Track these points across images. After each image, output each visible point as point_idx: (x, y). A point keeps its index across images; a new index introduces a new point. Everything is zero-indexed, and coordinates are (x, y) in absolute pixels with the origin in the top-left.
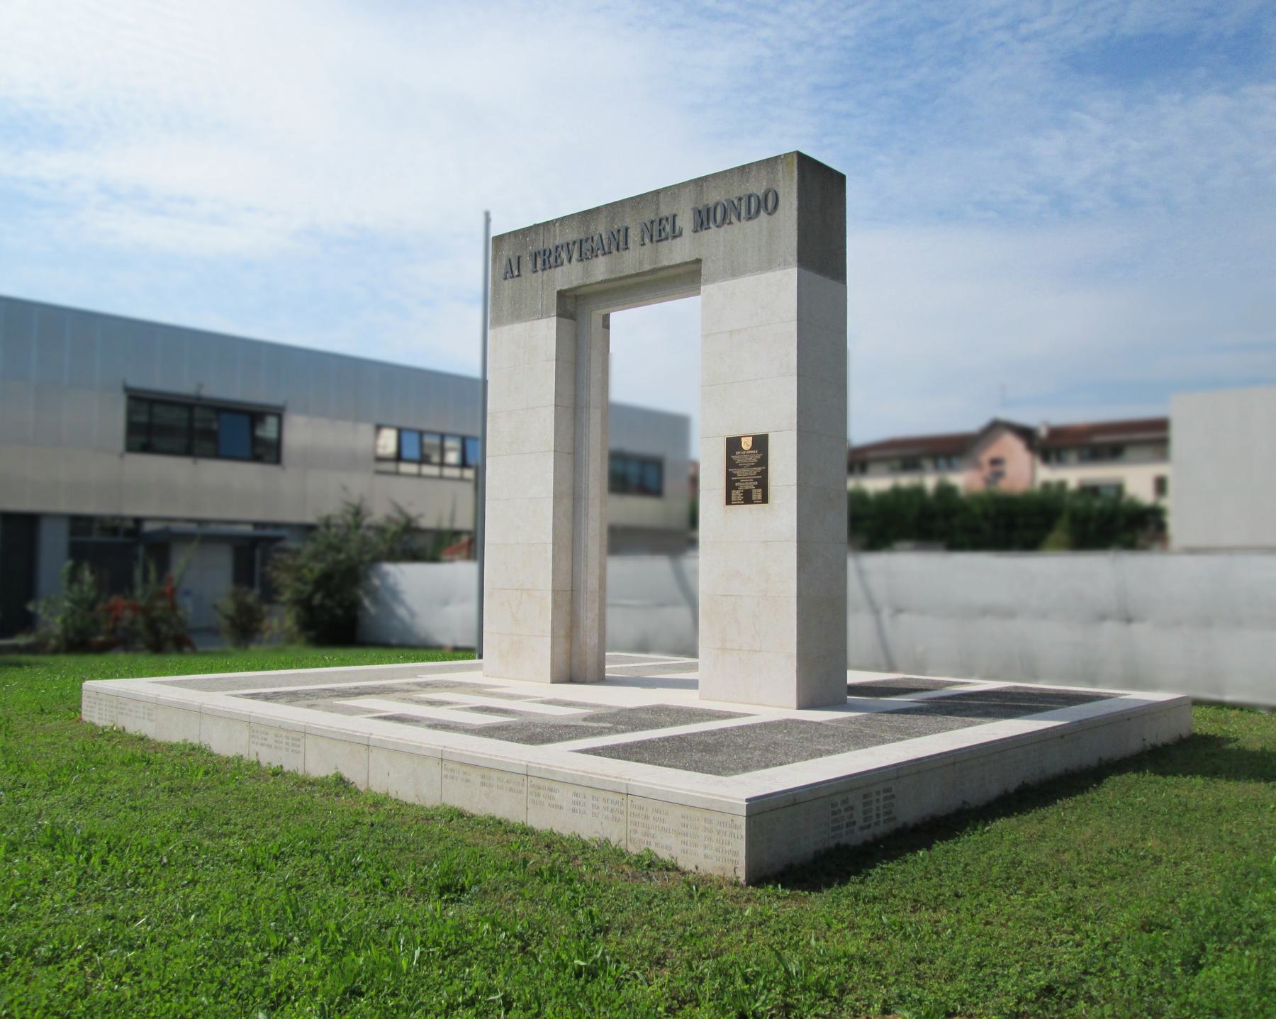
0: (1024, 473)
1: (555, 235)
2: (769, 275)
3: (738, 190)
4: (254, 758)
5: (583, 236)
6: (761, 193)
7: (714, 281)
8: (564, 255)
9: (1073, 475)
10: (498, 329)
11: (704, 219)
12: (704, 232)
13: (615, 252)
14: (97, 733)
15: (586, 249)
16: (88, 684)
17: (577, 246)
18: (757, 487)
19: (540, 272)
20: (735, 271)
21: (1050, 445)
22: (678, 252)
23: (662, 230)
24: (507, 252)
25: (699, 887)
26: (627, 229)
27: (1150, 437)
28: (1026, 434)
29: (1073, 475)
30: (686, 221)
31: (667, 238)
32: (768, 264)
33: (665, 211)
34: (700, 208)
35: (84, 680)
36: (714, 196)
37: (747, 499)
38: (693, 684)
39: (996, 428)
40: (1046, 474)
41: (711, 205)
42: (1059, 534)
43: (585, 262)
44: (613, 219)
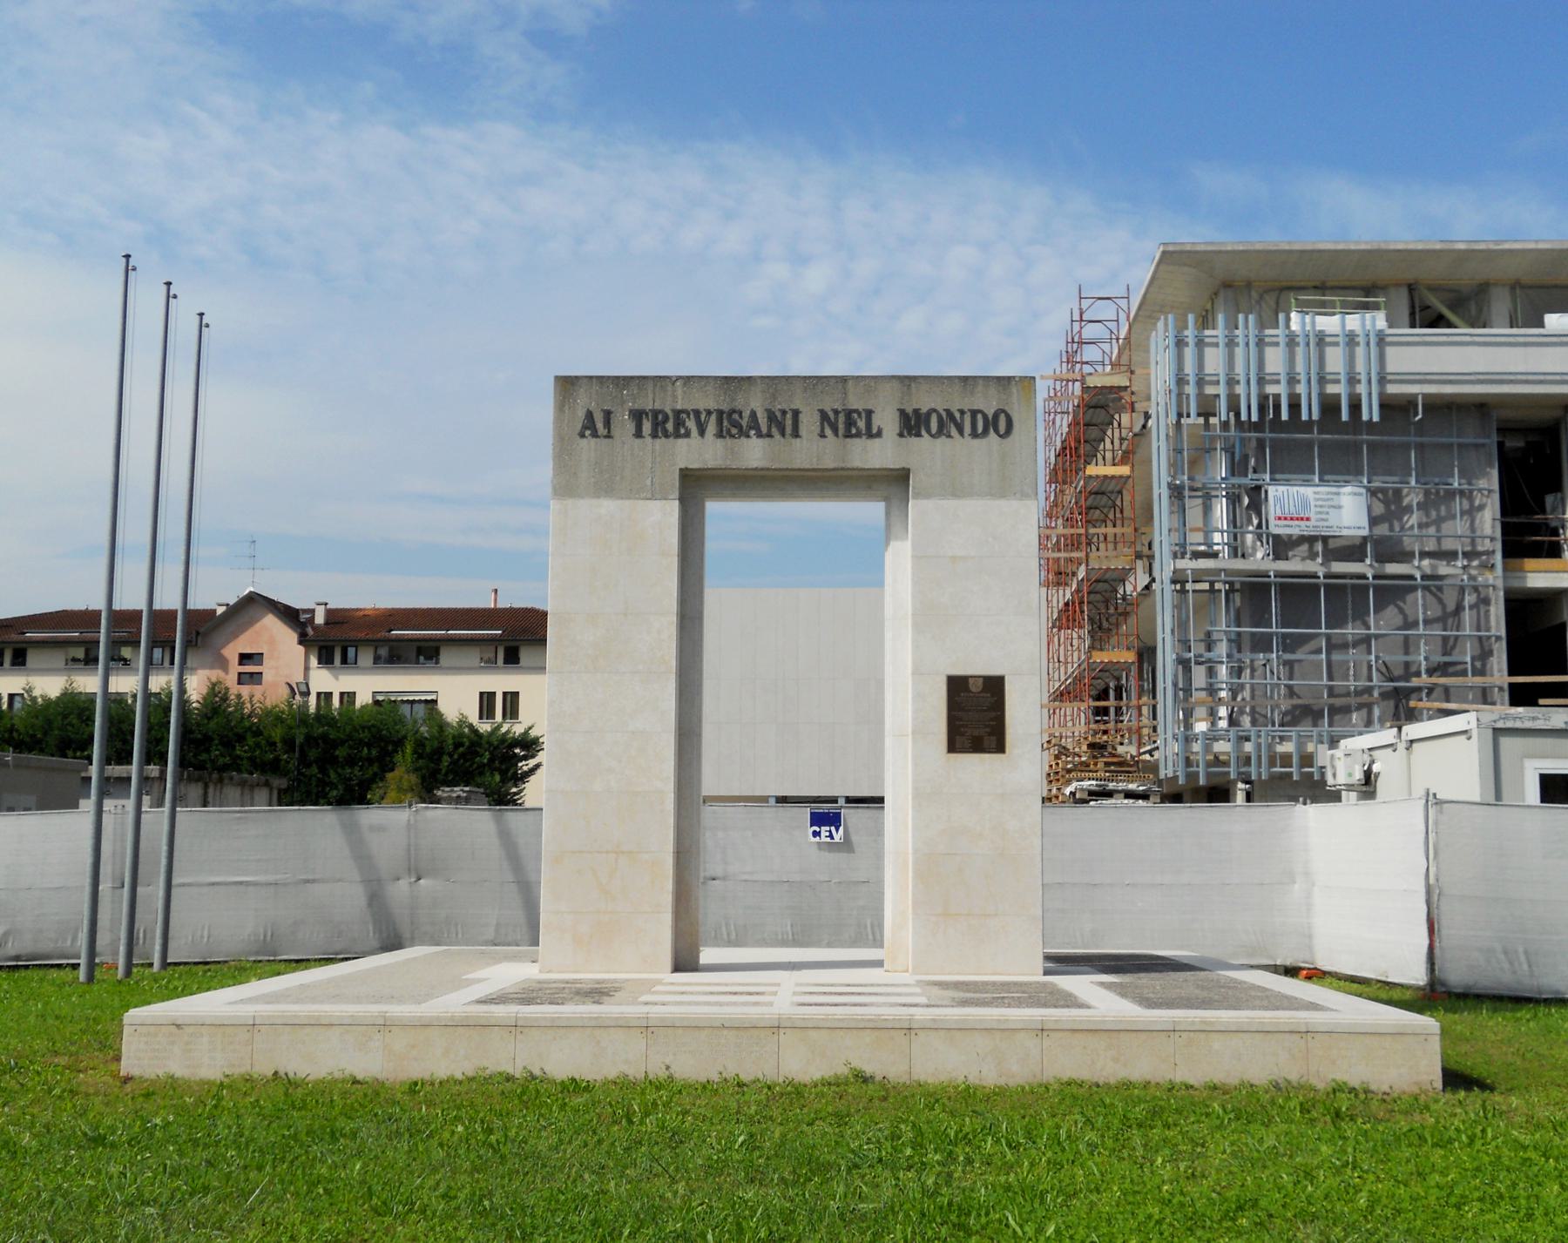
0: (287, 673)
1: (675, 397)
2: (1002, 503)
3: (958, 402)
4: (663, 1074)
5: (725, 407)
6: (990, 413)
7: (928, 496)
8: (691, 424)
9: (365, 685)
10: (569, 502)
11: (912, 424)
12: (914, 440)
13: (777, 436)
14: (151, 1091)
15: (731, 424)
16: (134, 1015)
17: (713, 417)
18: (990, 734)
19: (649, 440)
20: (957, 491)
21: (335, 637)
22: (881, 453)
23: (849, 423)
24: (584, 401)
25: (1417, 1103)
26: (796, 413)
27: (516, 636)
28: (290, 615)
29: (365, 685)
30: (887, 419)
31: (858, 435)
32: (1002, 488)
33: (855, 403)
34: (909, 410)
35: (127, 1008)
36: (924, 401)
37: (977, 747)
38: (879, 964)
39: (253, 604)
40: (324, 680)
41: (924, 410)
42: (402, 773)
43: (729, 441)
44: (774, 397)
